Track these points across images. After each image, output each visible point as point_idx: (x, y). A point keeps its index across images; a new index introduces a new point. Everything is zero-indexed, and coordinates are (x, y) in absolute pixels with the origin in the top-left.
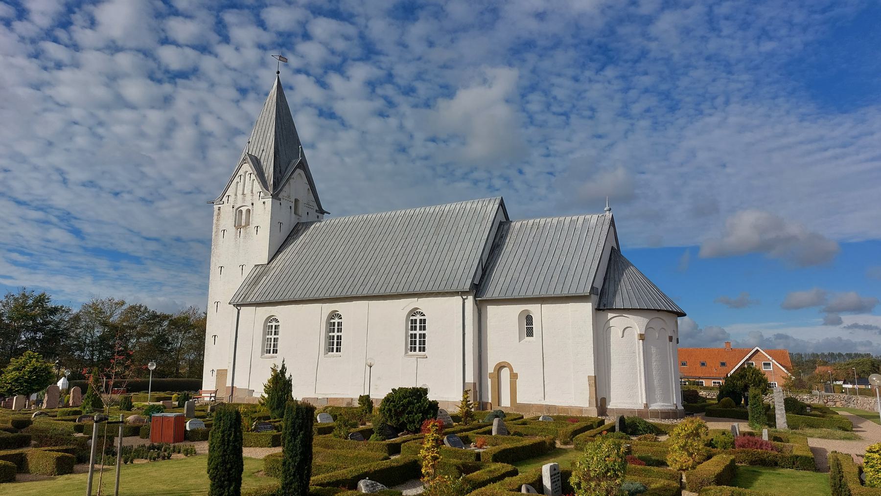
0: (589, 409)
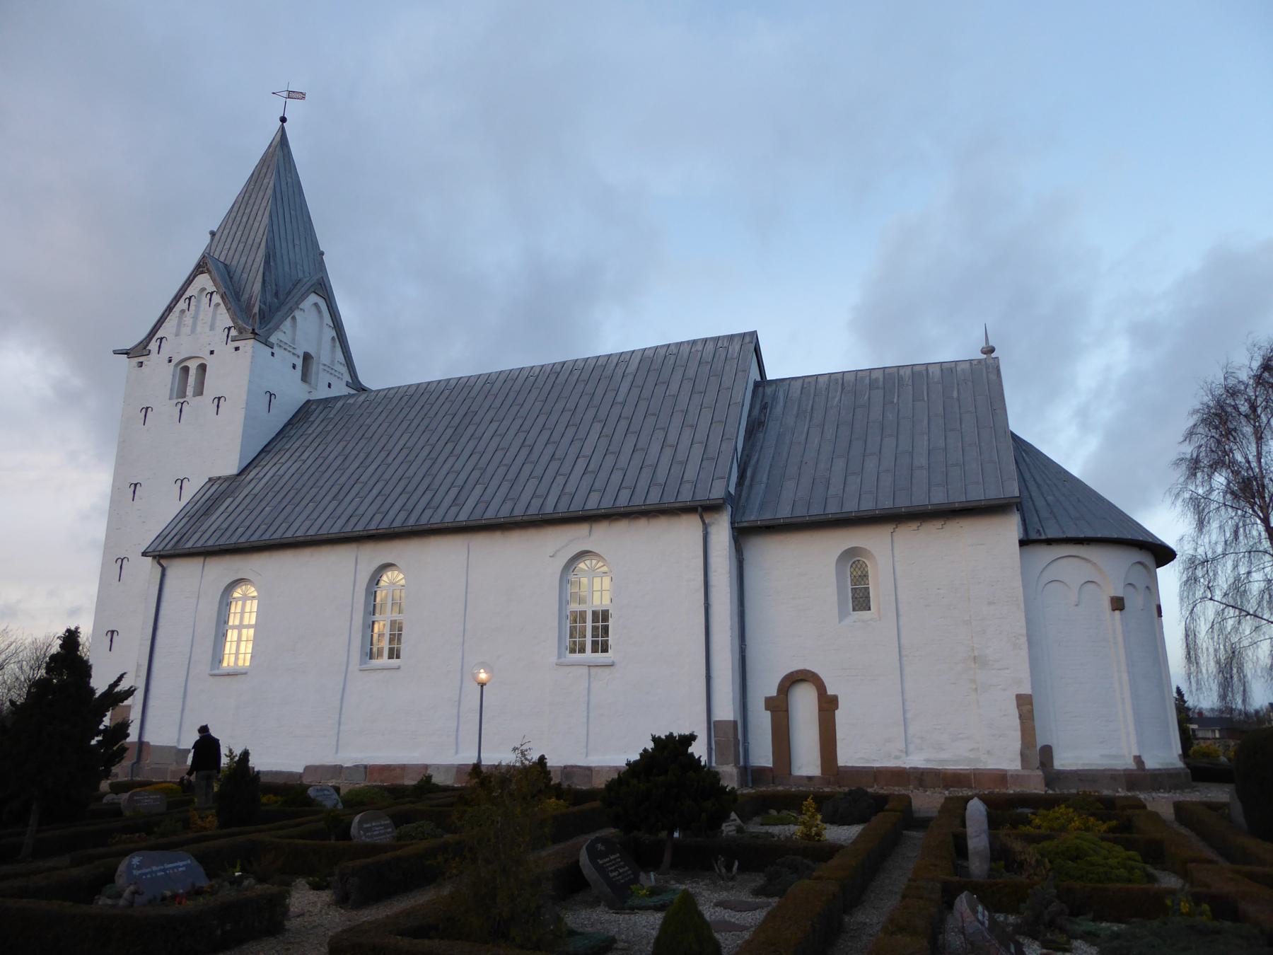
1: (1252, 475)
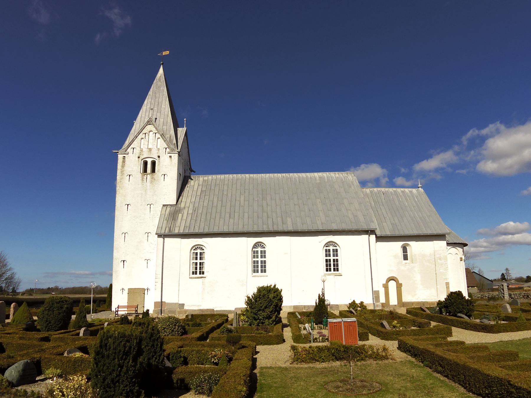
1: (289, 177)
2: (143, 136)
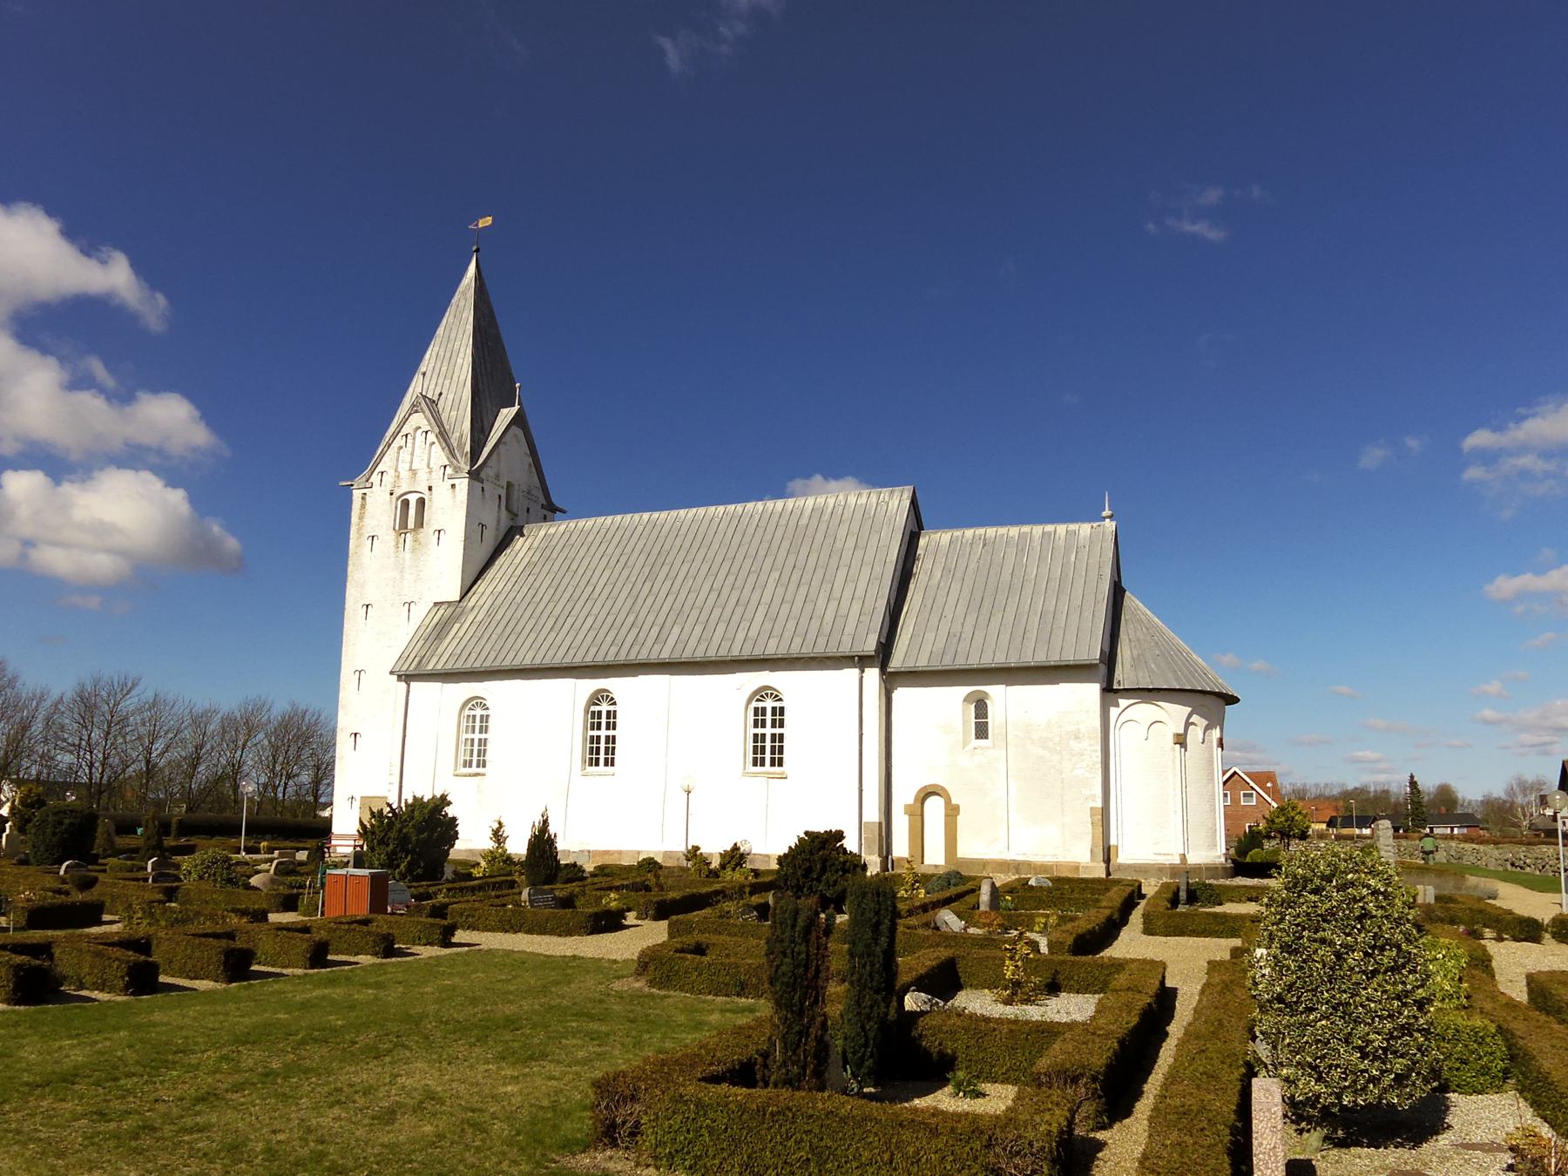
0: (1090, 865)
2: (399, 441)
